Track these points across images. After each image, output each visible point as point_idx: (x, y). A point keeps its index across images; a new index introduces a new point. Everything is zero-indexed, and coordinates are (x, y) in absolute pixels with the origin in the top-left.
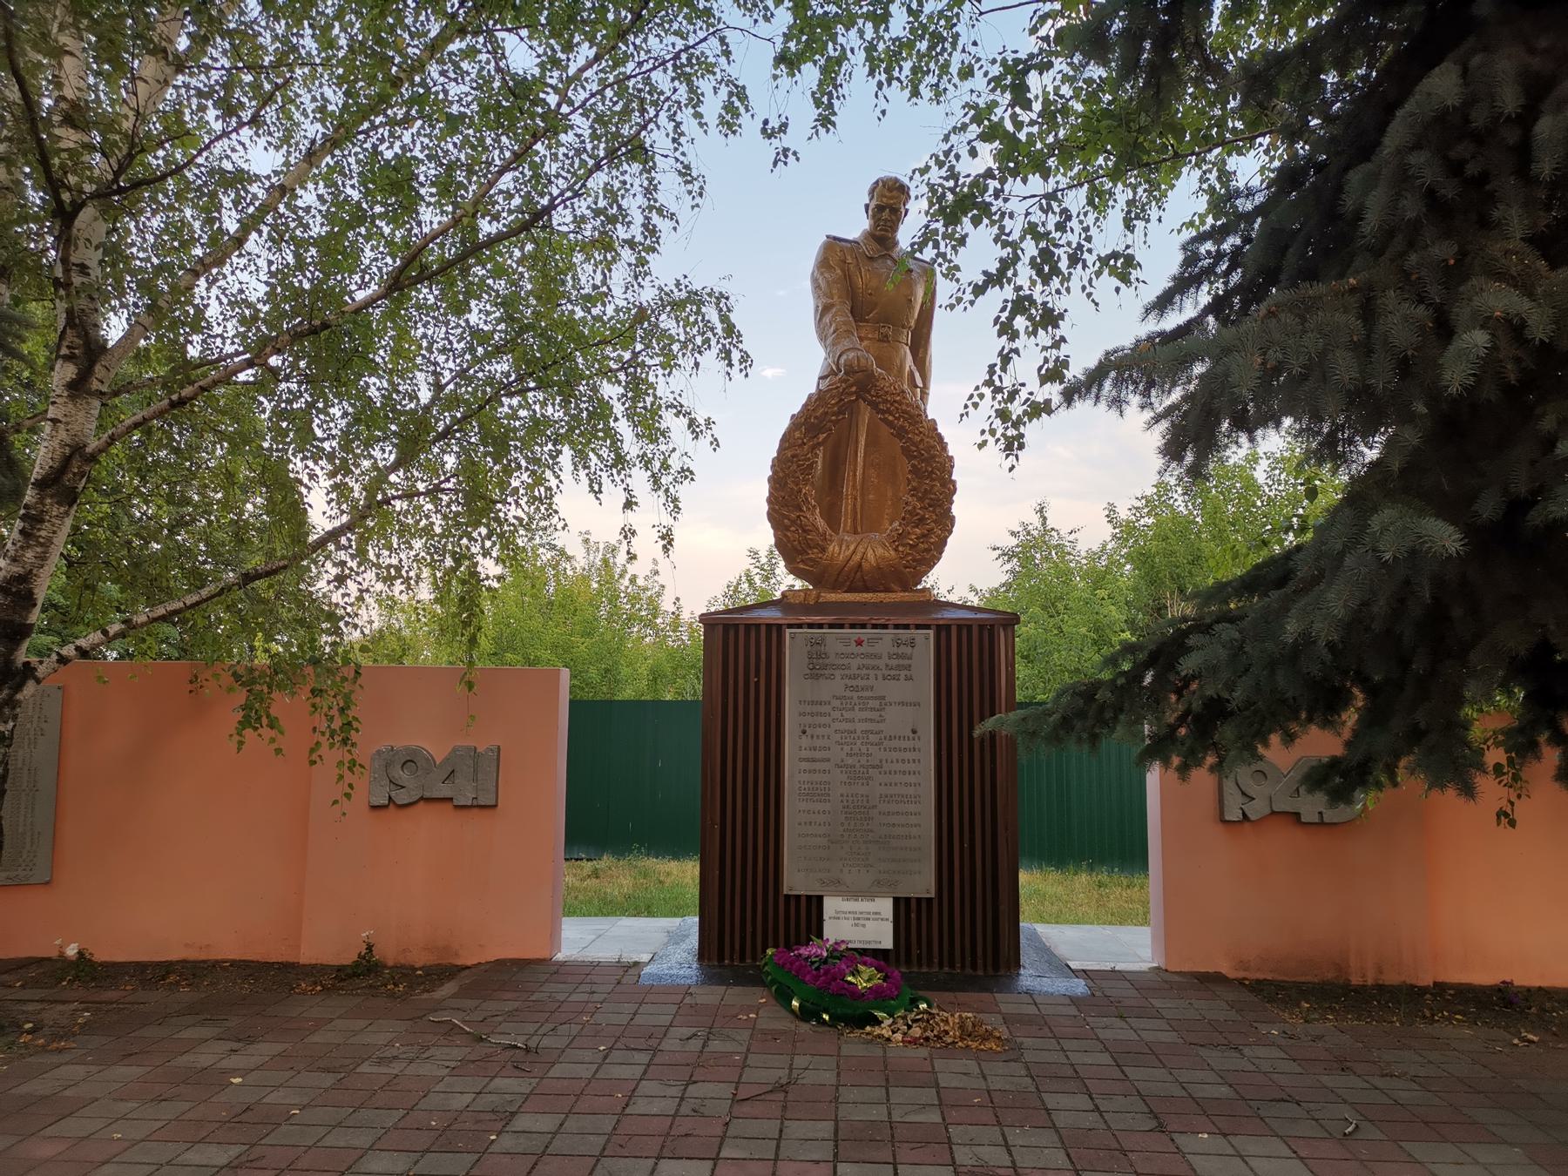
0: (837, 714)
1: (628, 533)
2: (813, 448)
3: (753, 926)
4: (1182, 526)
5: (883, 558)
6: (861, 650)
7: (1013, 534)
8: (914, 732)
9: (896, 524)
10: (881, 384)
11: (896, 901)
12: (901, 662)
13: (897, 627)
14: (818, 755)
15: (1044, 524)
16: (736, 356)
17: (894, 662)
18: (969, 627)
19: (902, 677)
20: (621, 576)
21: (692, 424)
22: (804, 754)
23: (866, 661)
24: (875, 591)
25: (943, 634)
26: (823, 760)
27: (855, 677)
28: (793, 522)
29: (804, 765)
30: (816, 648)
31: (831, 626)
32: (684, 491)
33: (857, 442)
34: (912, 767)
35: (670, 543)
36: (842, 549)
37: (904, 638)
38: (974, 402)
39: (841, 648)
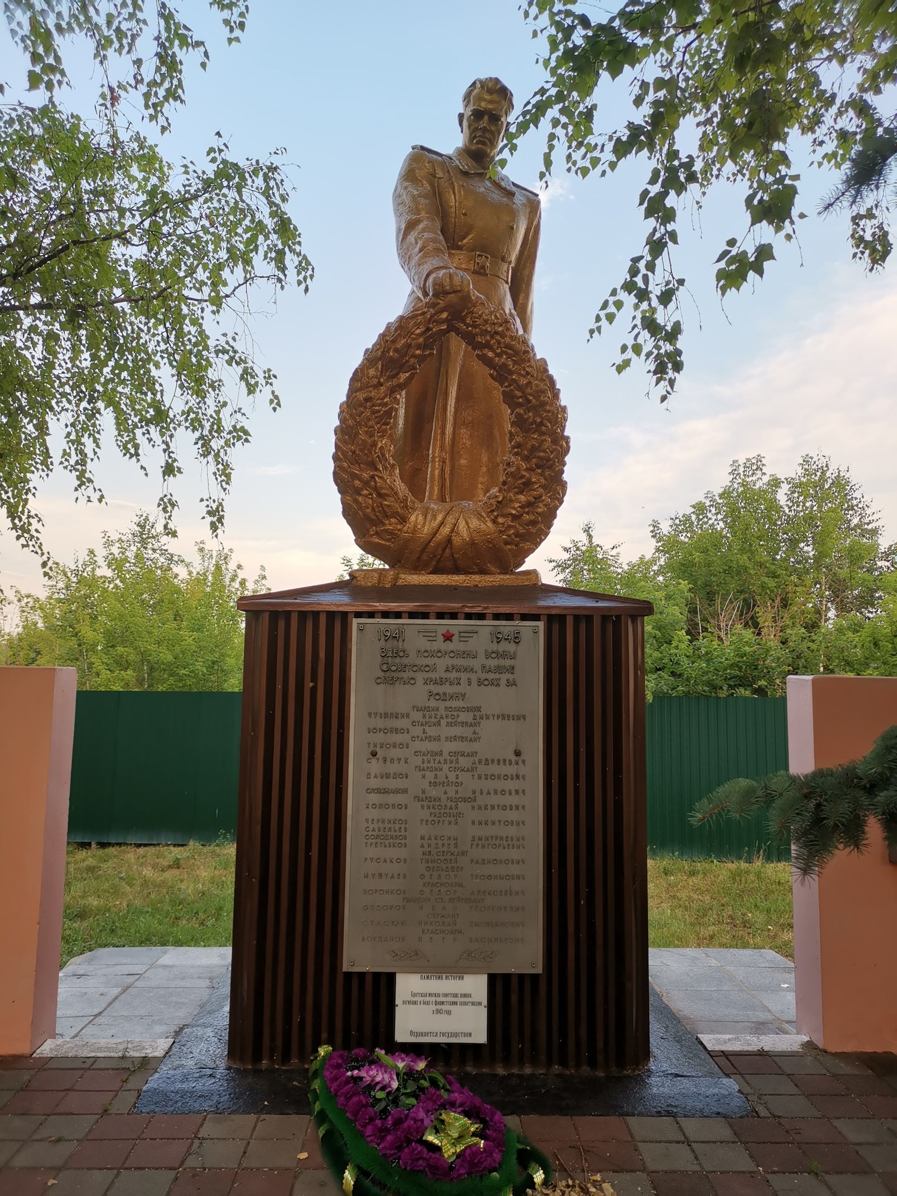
0: (417, 731)
1: (167, 504)
2: (393, 391)
3: (300, 1002)
4: (715, 540)
5: (478, 531)
6: (449, 646)
7: (566, 550)
8: (518, 753)
9: (494, 490)
10: (479, 310)
11: (493, 979)
12: (502, 662)
13: (497, 617)
14: (392, 784)
15: (590, 542)
16: (291, 260)
17: (493, 663)
18: (589, 619)
19: (503, 682)
20: (233, 580)
21: (247, 374)
22: (374, 783)
23: (459, 662)
24: (467, 573)
25: (556, 627)
26: (397, 791)
27: (441, 682)
28: (366, 484)
29: (375, 798)
30: (392, 643)
31: (412, 615)
32: (236, 455)
33: (446, 394)
34: (513, 800)
35: (220, 520)
36: (424, 521)
37: (506, 631)
38: (608, 313)
39: (422, 643)
